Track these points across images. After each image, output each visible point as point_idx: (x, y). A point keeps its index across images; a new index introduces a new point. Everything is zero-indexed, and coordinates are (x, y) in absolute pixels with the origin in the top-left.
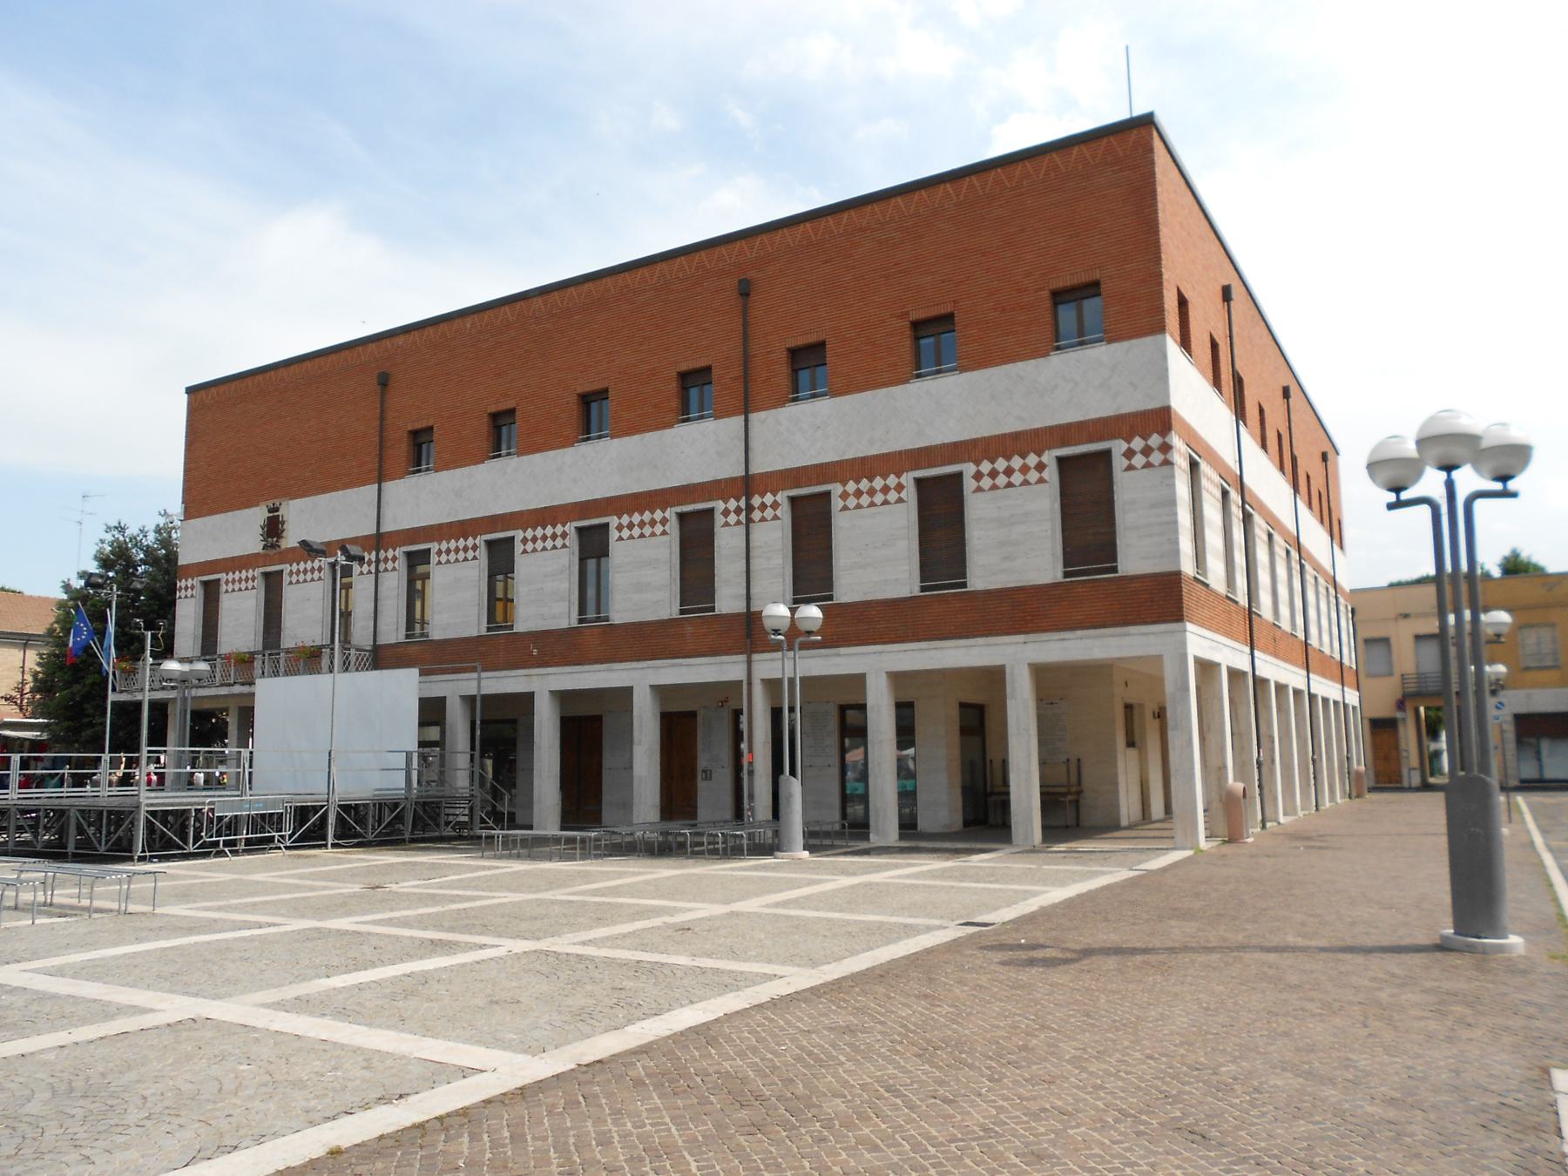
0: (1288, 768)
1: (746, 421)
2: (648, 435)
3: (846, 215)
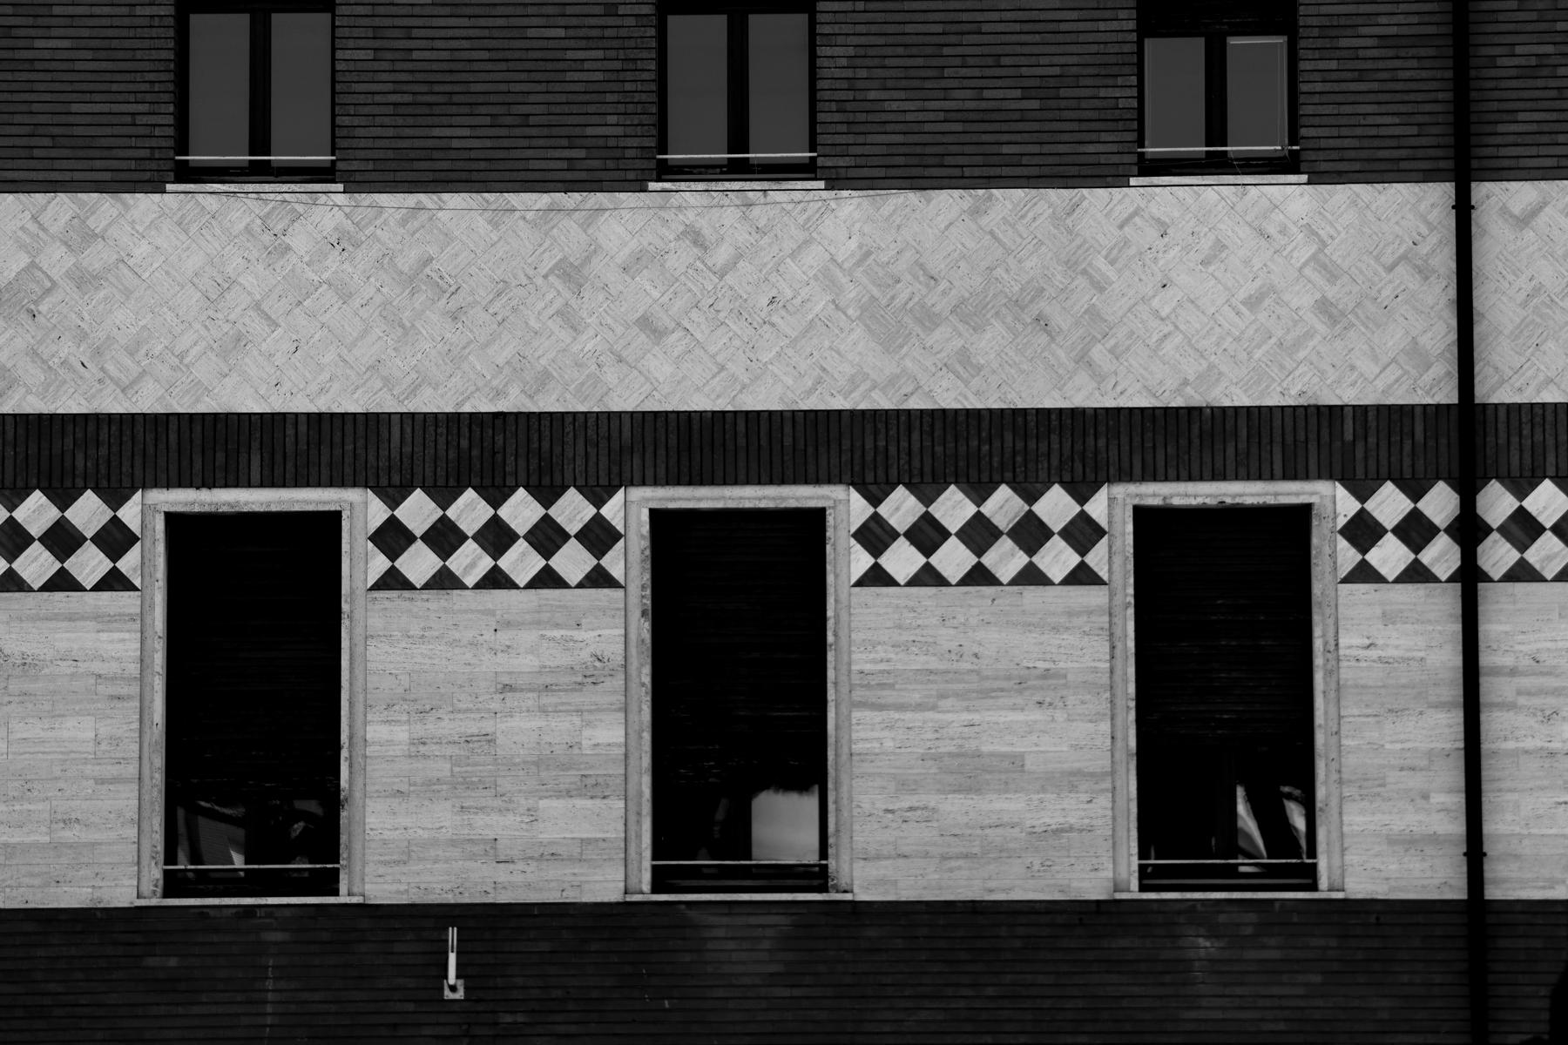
1: (1463, 210)
2: (1007, 200)
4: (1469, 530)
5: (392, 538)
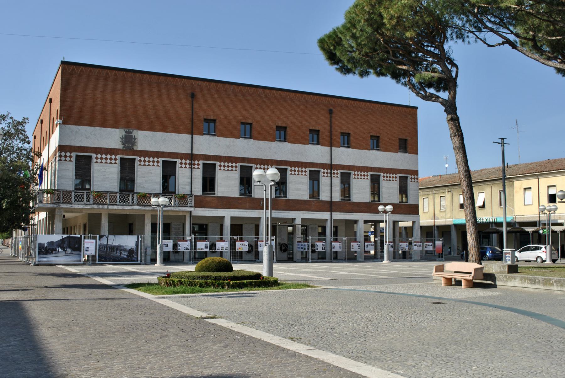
0: (159, 237)
2: (301, 145)
3: (356, 102)
4: (331, 173)
5: (140, 161)
